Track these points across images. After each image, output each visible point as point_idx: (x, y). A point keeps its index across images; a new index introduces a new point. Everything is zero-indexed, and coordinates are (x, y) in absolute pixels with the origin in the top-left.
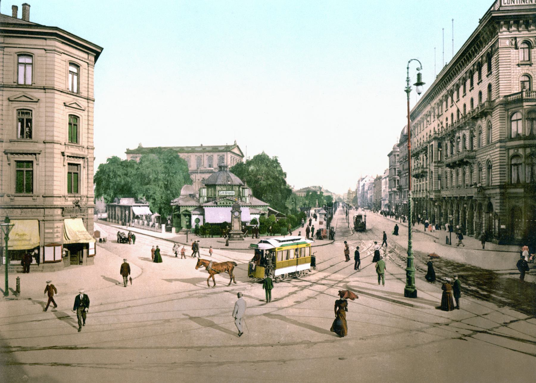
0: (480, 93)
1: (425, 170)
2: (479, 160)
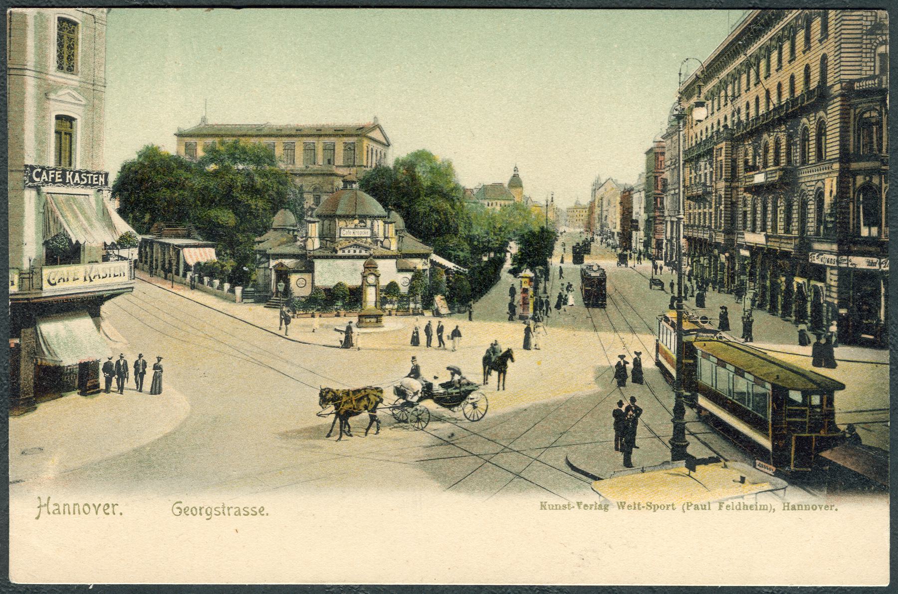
0: (807, 68)
1: (709, 189)
2: (803, 187)
